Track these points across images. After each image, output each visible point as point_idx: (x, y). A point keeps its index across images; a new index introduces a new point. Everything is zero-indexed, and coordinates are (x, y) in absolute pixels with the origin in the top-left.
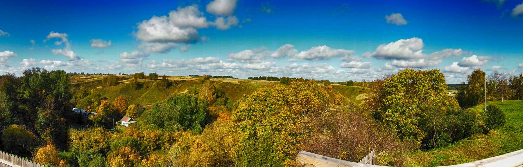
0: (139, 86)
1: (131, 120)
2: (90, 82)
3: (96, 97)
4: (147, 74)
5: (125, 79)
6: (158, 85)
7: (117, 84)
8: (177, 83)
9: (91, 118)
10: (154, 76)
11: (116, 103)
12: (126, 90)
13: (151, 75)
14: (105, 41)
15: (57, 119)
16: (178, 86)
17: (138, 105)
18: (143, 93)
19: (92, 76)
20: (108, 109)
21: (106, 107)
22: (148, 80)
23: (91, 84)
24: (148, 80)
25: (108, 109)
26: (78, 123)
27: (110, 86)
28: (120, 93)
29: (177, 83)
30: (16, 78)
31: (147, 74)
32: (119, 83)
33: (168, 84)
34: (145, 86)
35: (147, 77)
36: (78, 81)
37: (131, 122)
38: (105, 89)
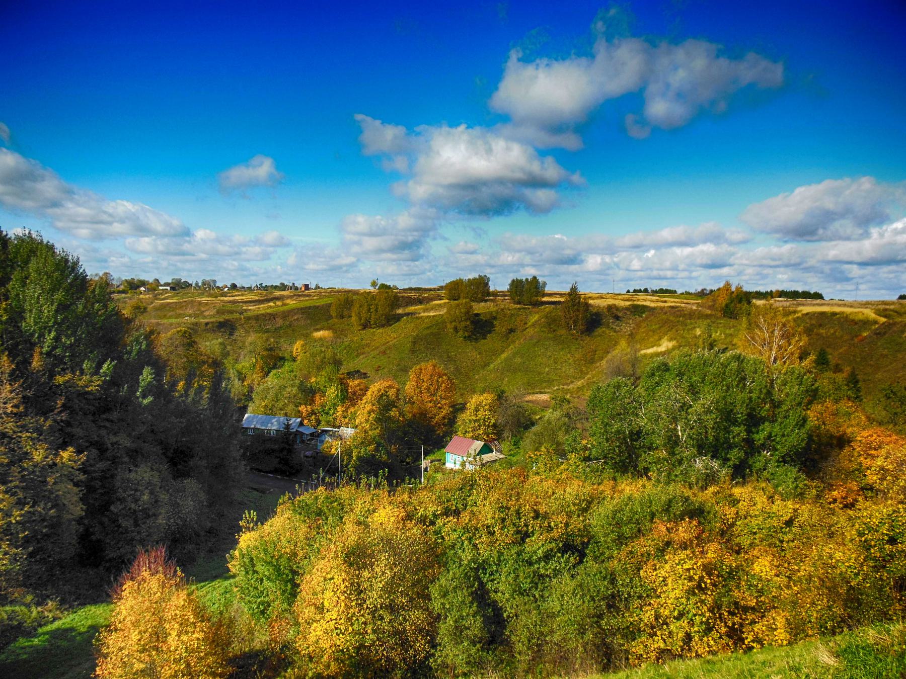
0: (479, 327)
1: (486, 449)
2: (273, 316)
3: (329, 368)
4: (500, 284)
5: (420, 301)
6: (551, 323)
7: (391, 319)
8: (617, 318)
9: (334, 447)
10: (527, 292)
11: (416, 387)
12: (430, 341)
13: (517, 286)
14: (477, 131)
15: (38, 456)
16: (626, 328)
17: (501, 396)
18: (496, 353)
19: (267, 293)
20: (394, 413)
21: (385, 405)
22: (507, 304)
23: (280, 322)
24: (507, 304)
25: (394, 413)
26: (276, 471)
27: (365, 326)
28: (413, 351)
29: (617, 318)
30: (480, 125)
31: (500, 284)
32: (398, 318)
33: (585, 320)
34: (499, 327)
35: (503, 294)
36: (219, 312)
37: (487, 457)
38: (347, 341)
